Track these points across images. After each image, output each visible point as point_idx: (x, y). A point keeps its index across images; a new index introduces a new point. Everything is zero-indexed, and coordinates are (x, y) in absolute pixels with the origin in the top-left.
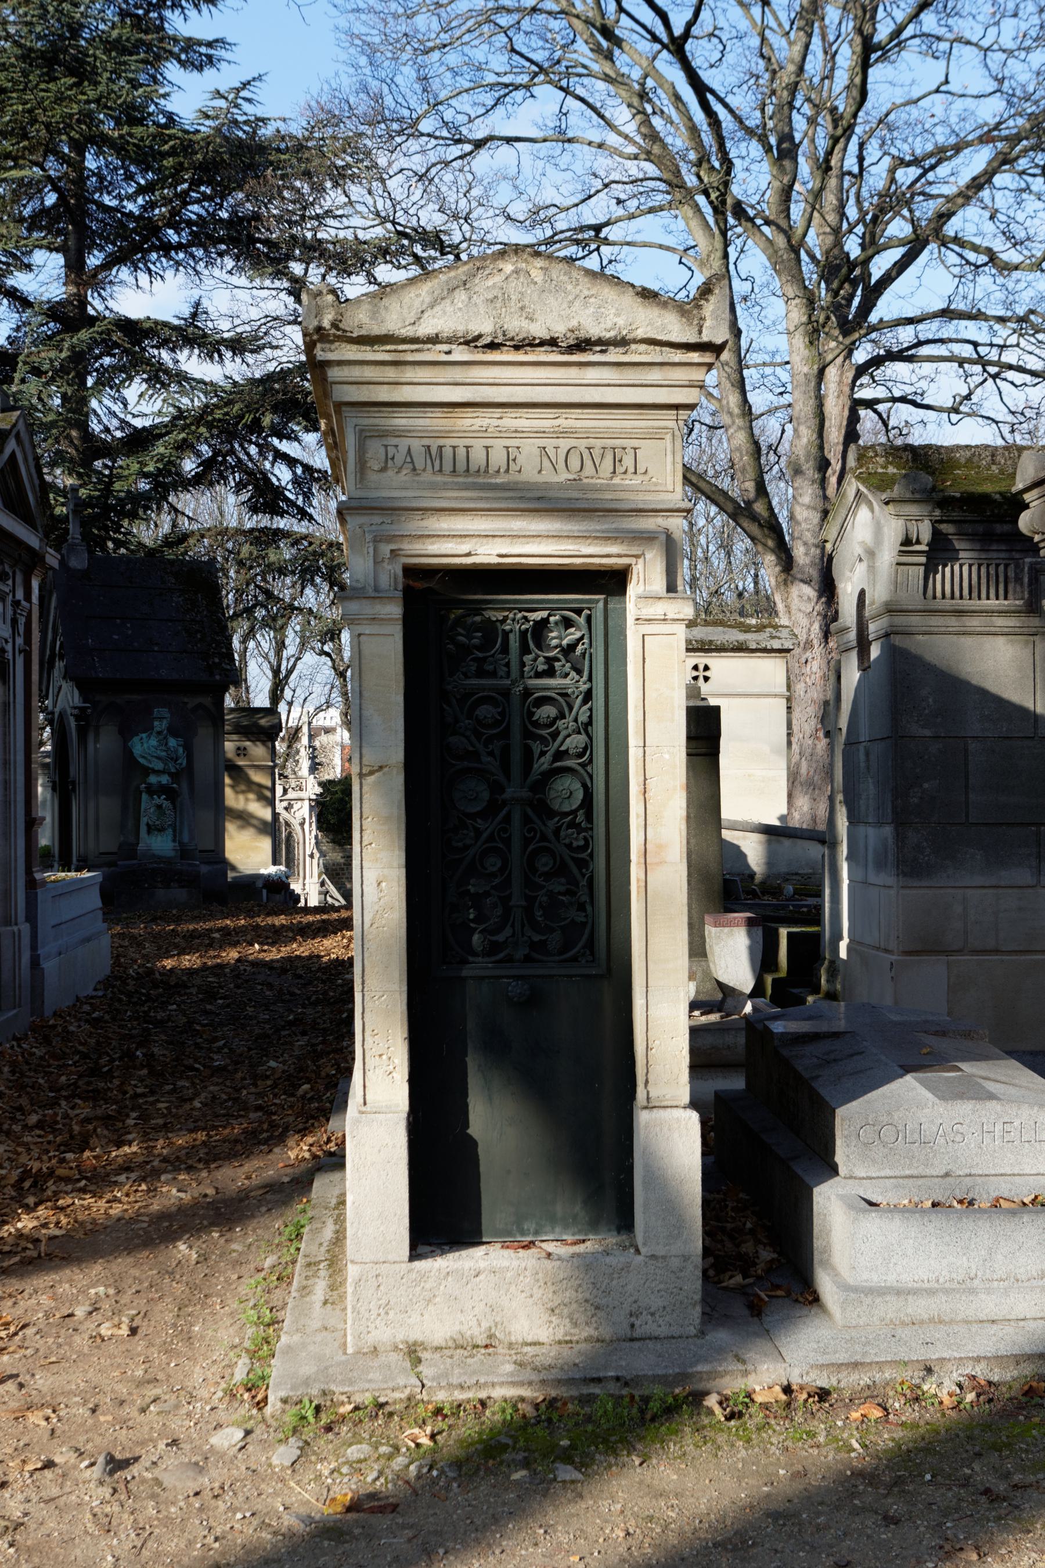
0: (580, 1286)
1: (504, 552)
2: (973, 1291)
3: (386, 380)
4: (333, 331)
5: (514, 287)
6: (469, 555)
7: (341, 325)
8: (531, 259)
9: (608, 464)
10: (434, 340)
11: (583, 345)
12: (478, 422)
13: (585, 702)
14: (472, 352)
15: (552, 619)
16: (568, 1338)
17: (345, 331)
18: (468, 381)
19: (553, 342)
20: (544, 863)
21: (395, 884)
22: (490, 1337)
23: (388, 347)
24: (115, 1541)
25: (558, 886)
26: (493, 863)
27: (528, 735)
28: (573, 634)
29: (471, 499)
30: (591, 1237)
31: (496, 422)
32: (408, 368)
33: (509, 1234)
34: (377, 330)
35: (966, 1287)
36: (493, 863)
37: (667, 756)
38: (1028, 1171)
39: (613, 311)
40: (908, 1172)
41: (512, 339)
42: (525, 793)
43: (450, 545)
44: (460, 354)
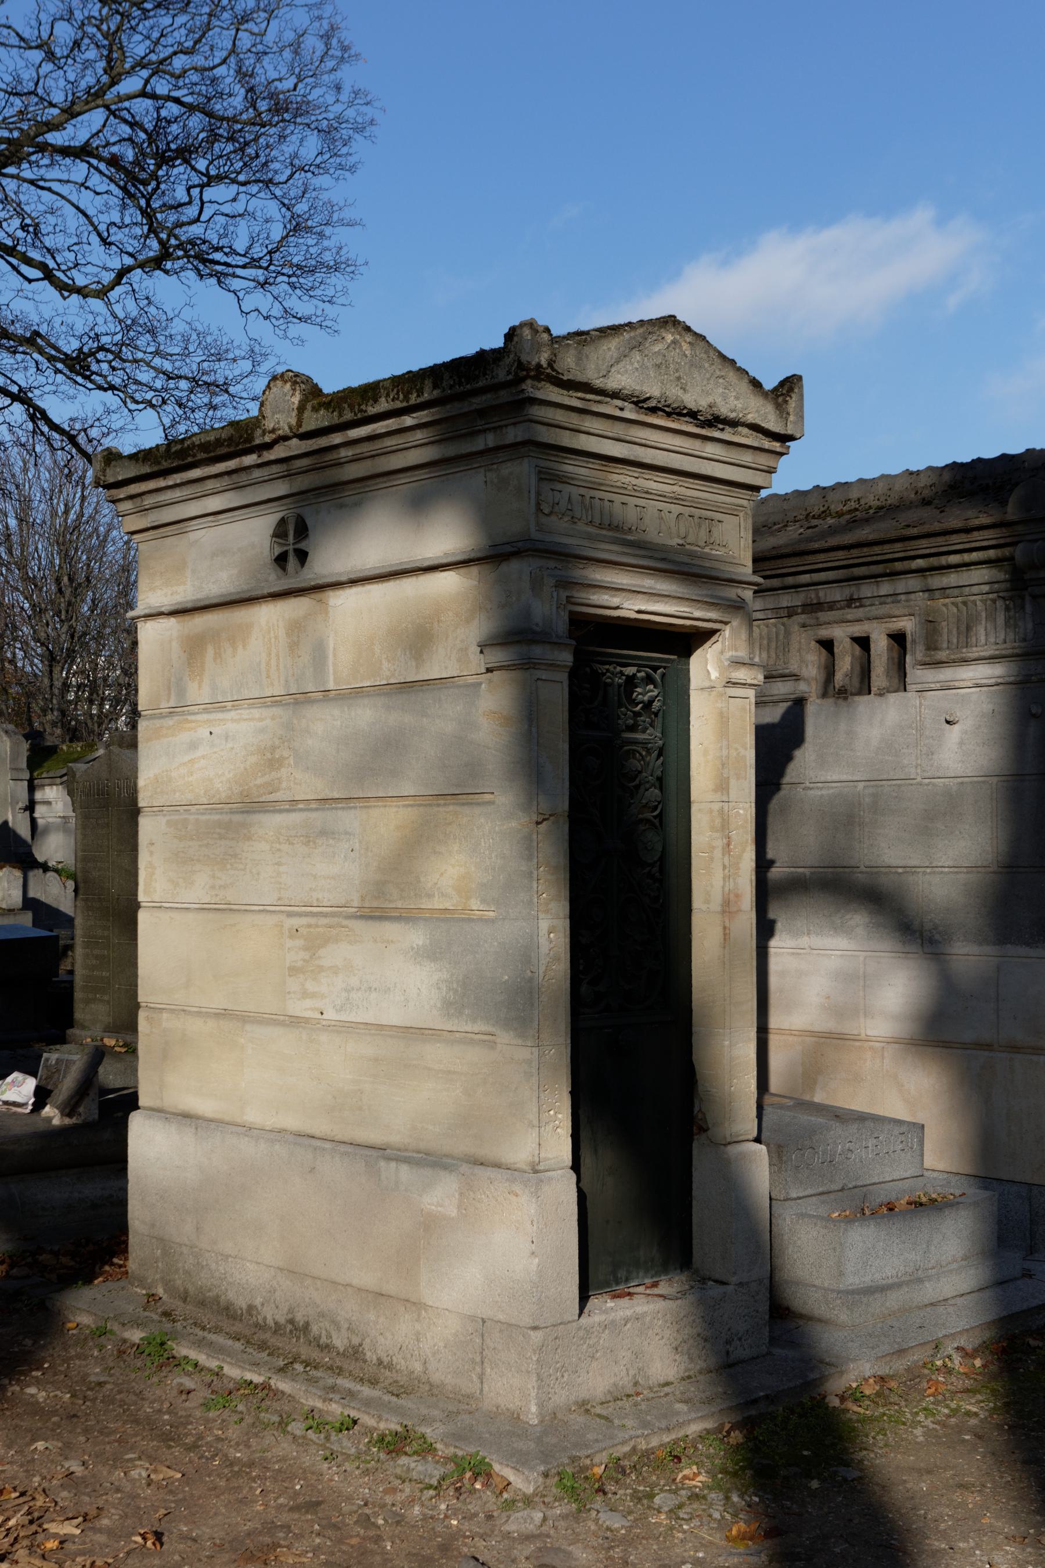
0: (694, 1321)
1: (643, 608)
2: (920, 1281)
3: (571, 426)
4: (549, 371)
6: (617, 608)
7: (555, 366)
8: (683, 333)
10: (615, 395)
11: (716, 421)
12: (641, 482)
13: (660, 755)
14: (638, 412)
15: (639, 675)
16: (687, 1374)
17: (558, 373)
18: (628, 438)
19: (693, 414)
21: (562, 935)
22: (636, 1384)
23: (580, 395)
29: (617, 553)
30: (663, 1278)
31: (634, 481)
32: (588, 417)
33: (609, 1285)
35: (915, 1280)
37: (741, 812)
38: (887, 1179)
39: (734, 394)
40: (821, 1189)
41: (668, 406)
43: (606, 597)
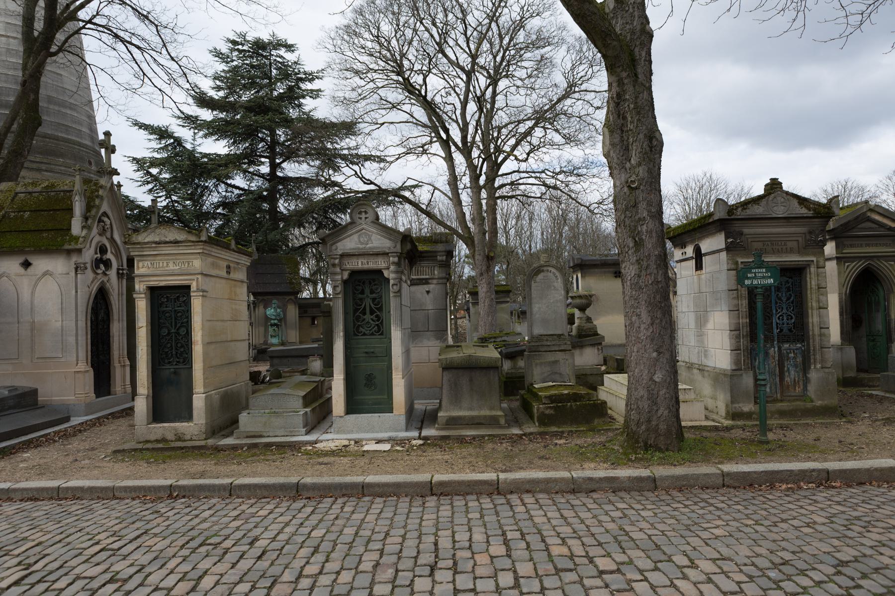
20: (179, 345)
26: (169, 345)
36: (169, 345)
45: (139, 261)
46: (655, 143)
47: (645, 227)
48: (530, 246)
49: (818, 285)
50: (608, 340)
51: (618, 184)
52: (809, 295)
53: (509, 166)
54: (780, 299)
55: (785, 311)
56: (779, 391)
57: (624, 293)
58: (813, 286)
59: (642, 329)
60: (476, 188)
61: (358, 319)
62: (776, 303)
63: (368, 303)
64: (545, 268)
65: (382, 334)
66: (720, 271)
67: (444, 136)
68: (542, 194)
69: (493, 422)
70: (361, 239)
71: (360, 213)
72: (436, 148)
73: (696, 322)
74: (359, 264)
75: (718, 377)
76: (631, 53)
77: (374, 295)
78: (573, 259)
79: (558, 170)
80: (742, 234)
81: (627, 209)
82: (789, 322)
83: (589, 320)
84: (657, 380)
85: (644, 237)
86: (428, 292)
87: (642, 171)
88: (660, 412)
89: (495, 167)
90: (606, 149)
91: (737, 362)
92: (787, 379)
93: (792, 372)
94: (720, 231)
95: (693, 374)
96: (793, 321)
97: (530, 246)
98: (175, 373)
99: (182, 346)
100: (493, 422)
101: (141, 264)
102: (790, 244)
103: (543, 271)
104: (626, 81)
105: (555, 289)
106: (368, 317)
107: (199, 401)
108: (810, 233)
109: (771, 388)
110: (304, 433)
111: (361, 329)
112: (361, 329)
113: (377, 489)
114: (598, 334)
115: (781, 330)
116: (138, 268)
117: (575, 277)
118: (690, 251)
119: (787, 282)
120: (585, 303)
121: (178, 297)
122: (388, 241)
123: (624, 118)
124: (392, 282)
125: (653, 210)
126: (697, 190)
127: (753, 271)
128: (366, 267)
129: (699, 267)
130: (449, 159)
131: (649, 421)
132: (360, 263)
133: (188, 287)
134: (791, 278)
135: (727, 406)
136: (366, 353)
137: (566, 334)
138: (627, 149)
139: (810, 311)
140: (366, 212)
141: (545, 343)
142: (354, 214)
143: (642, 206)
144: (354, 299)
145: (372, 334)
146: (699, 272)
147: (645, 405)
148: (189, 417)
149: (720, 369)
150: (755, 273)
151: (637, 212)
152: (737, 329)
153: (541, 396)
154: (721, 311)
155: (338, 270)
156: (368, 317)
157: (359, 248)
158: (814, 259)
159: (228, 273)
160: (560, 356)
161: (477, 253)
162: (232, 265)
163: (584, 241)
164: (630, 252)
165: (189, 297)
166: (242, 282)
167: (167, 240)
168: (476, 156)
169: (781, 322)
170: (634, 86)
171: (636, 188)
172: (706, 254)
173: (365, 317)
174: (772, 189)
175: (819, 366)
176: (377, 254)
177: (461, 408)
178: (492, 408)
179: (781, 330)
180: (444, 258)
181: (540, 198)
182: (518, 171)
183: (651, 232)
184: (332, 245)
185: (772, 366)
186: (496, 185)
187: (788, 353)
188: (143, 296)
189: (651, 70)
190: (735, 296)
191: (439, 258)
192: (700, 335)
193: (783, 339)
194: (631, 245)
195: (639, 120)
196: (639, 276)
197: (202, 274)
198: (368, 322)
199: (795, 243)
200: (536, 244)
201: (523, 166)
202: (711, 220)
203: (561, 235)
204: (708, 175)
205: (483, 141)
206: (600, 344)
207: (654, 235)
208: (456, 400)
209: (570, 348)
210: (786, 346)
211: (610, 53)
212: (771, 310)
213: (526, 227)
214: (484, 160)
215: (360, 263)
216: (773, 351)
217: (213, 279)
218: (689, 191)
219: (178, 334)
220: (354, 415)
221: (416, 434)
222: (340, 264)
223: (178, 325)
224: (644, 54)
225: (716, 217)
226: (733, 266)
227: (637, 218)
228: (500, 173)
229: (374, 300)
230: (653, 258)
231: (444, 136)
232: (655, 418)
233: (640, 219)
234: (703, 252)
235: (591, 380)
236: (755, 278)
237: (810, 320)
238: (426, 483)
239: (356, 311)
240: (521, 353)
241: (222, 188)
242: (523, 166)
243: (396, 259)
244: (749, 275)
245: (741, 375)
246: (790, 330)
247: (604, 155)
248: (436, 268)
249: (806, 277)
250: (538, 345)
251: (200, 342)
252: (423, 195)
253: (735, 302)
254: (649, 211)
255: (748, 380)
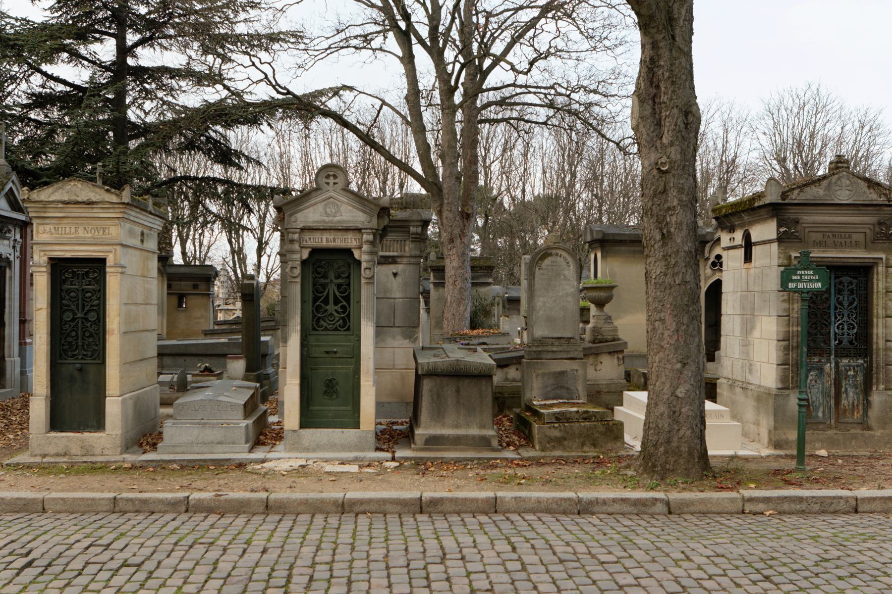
5: (74, 188)
9: (101, 232)
20: (87, 334)
24: (456, 328)
25: (91, 340)
26: (74, 334)
27: (83, 300)
28: (96, 275)
34: (38, 199)
36: (74, 334)
42: (82, 316)
44: (60, 205)
45: (39, 224)
46: (691, 119)
47: (674, 219)
48: (523, 191)
49: (886, 288)
50: (630, 348)
51: (647, 163)
52: (875, 301)
53: (498, 76)
54: (841, 303)
55: (846, 318)
56: (833, 415)
57: (647, 293)
58: (880, 289)
59: (666, 335)
60: (448, 108)
61: (318, 309)
62: (836, 308)
63: (332, 289)
64: (554, 251)
65: (348, 329)
66: (770, 266)
67: (403, 25)
68: (549, 118)
69: (483, 443)
70: (328, 210)
71: (328, 177)
72: (392, 43)
73: (742, 329)
74: (324, 241)
75: (761, 397)
76: (669, 12)
77: (340, 281)
78: (592, 231)
79: (574, 83)
80: (797, 222)
81: (655, 195)
82: (851, 332)
83: (608, 318)
84: (680, 395)
85: (672, 230)
86: (395, 275)
87: (674, 153)
88: (682, 432)
89: (477, 74)
90: (635, 123)
91: (784, 379)
92: (844, 402)
93: (851, 394)
94: (772, 217)
95: (735, 394)
96: (855, 331)
97: (523, 191)
98: (80, 370)
99: (91, 336)
100: (483, 443)
101: (41, 228)
102: (855, 237)
103: (551, 255)
104: (662, 44)
105: (566, 278)
106: (331, 308)
107: (114, 407)
108: (880, 223)
109: (824, 412)
110: (247, 450)
111: (322, 322)
112: (322, 322)
113: (593, 350)
114: (619, 339)
115: (840, 342)
116: (38, 232)
117: (592, 256)
118: (738, 236)
119: (851, 283)
120: (602, 296)
121: (87, 273)
122: (361, 214)
123: (658, 87)
124: (364, 265)
125: (685, 198)
126: (795, 110)
127: (799, 272)
128: (332, 245)
129: (748, 258)
130: (408, 60)
131: (668, 442)
132: (324, 240)
133: (103, 261)
134: (856, 278)
135: (770, 432)
136: (327, 352)
137: (578, 338)
138: (659, 124)
139: (875, 320)
140: (335, 177)
141: (550, 348)
142: (319, 179)
143: (673, 193)
144: (314, 285)
145: (336, 329)
146: (747, 265)
147: (665, 424)
148: (99, 424)
149: (766, 388)
150: (801, 275)
151: (666, 201)
152: (786, 339)
153: (542, 413)
154: (770, 316)
155: (296, 247)
156: (331, 308)
157: (324, 222)
158: (883, 256)
159: (142, 241)
160: (567, 366)
161: (445, 208)
162: (145, 231)
163: (610, 185)
164: (656, 246)
165: (104, 274)
166: (154, 253)
167: (79, 199)
168: (452, 59)
169: (840, 332)
170: (671, 50)
171: (667, 172)
172: (756, 244)
173: (327, 307)
174: (837, 168)
175: (882, 387)
176: (347, 230)
177: (443, 425)
178: (482, 426)
179: (840, 342)
180: (420, 229)
181: (545, 123)
182: (514, 85)
183: (681, 224)
184: (291, 215)
185: (827, 385)
186: (478, 104)
187: (847, 371)
188: (44, 269)
189: (692, 29)
190: (785, 297)
191: (412, 229)
192: (746, 344)
193: (842, 352)
194: (658, 237)
195: (674, 91)
196: (666, 275)
197: (122, 245)
198: (331, 314)
199: (862, 236)
200: (533, 187)
201: (522, 79)
202: (761, 203)
203: (574, 175)
204: (814, 88)
205: (461, 32)
206: (622, 351)
207: (684, 227)
208: (439, 415)
209: (581, 356)
210: (845, 361)
211: (644, 11)
212: (829, 317)
213: (523, 167)
214: (463, 66)
215: (324, 240)
216: (830, 368)
217: (130, 250)
218: (783, 112)
219: (87, 320)
220: (311, 430)
221: (389, 455)
222: (299, 241)
223: (87, 309)
224: (683, 12)
225: (767, 200)
226: (785, 262)
227: (666, 206)
228: (484, 87)
229: (339, 286)
230: (682, 254)
231: (403, 25)
232: (675, 439)
233: (669, 209)
234: (753, 240)
235: (606, 398)
236: (800, 281)
237: (875, 331)
238: (415, 500)
239: (315, 300)
240: (518, 361)
241: (37, 80)
242: (522, 79)
243: (371, 237)
244: (794, 278)
245: (788, 395)
246: (851, 342)
247: (633, 129)
248: (407, 243)
249: (873, 279)
250: (539, 350)
251: (116, 332)
252: (359, 109)
253: (786, 305)
254: (680, 200)
255: (793, 401)
